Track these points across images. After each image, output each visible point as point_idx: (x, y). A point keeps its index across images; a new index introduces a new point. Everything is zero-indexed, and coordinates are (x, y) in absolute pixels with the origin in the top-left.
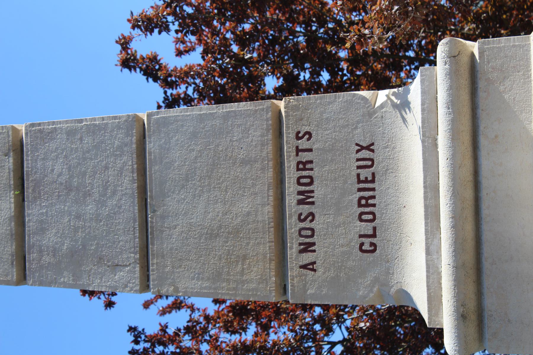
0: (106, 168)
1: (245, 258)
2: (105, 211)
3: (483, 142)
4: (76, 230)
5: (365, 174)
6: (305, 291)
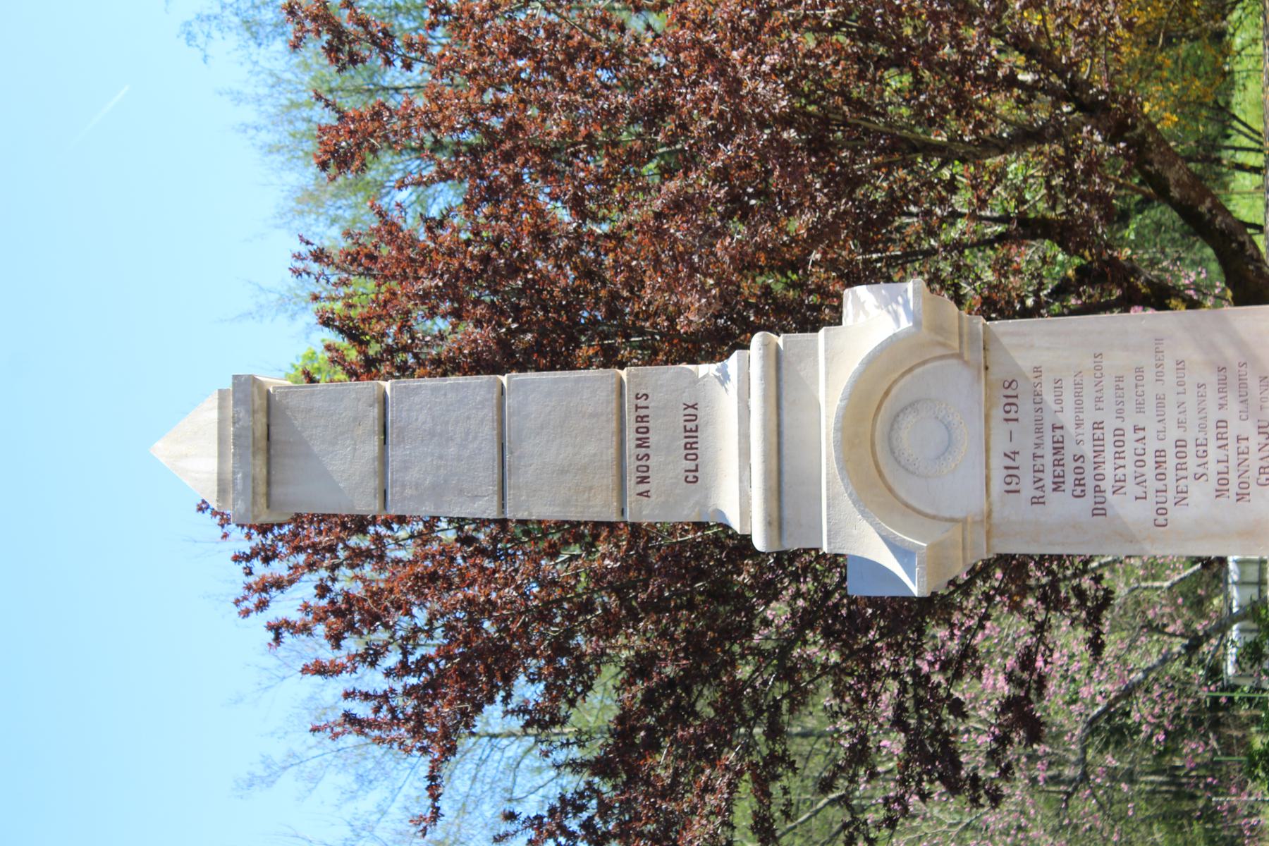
0: (468, 418)
1: (591, 488)
2: (466, 453)
3: (785, 404)
4: (438, 468)
5: (690, 425)
6: (641, 512)
